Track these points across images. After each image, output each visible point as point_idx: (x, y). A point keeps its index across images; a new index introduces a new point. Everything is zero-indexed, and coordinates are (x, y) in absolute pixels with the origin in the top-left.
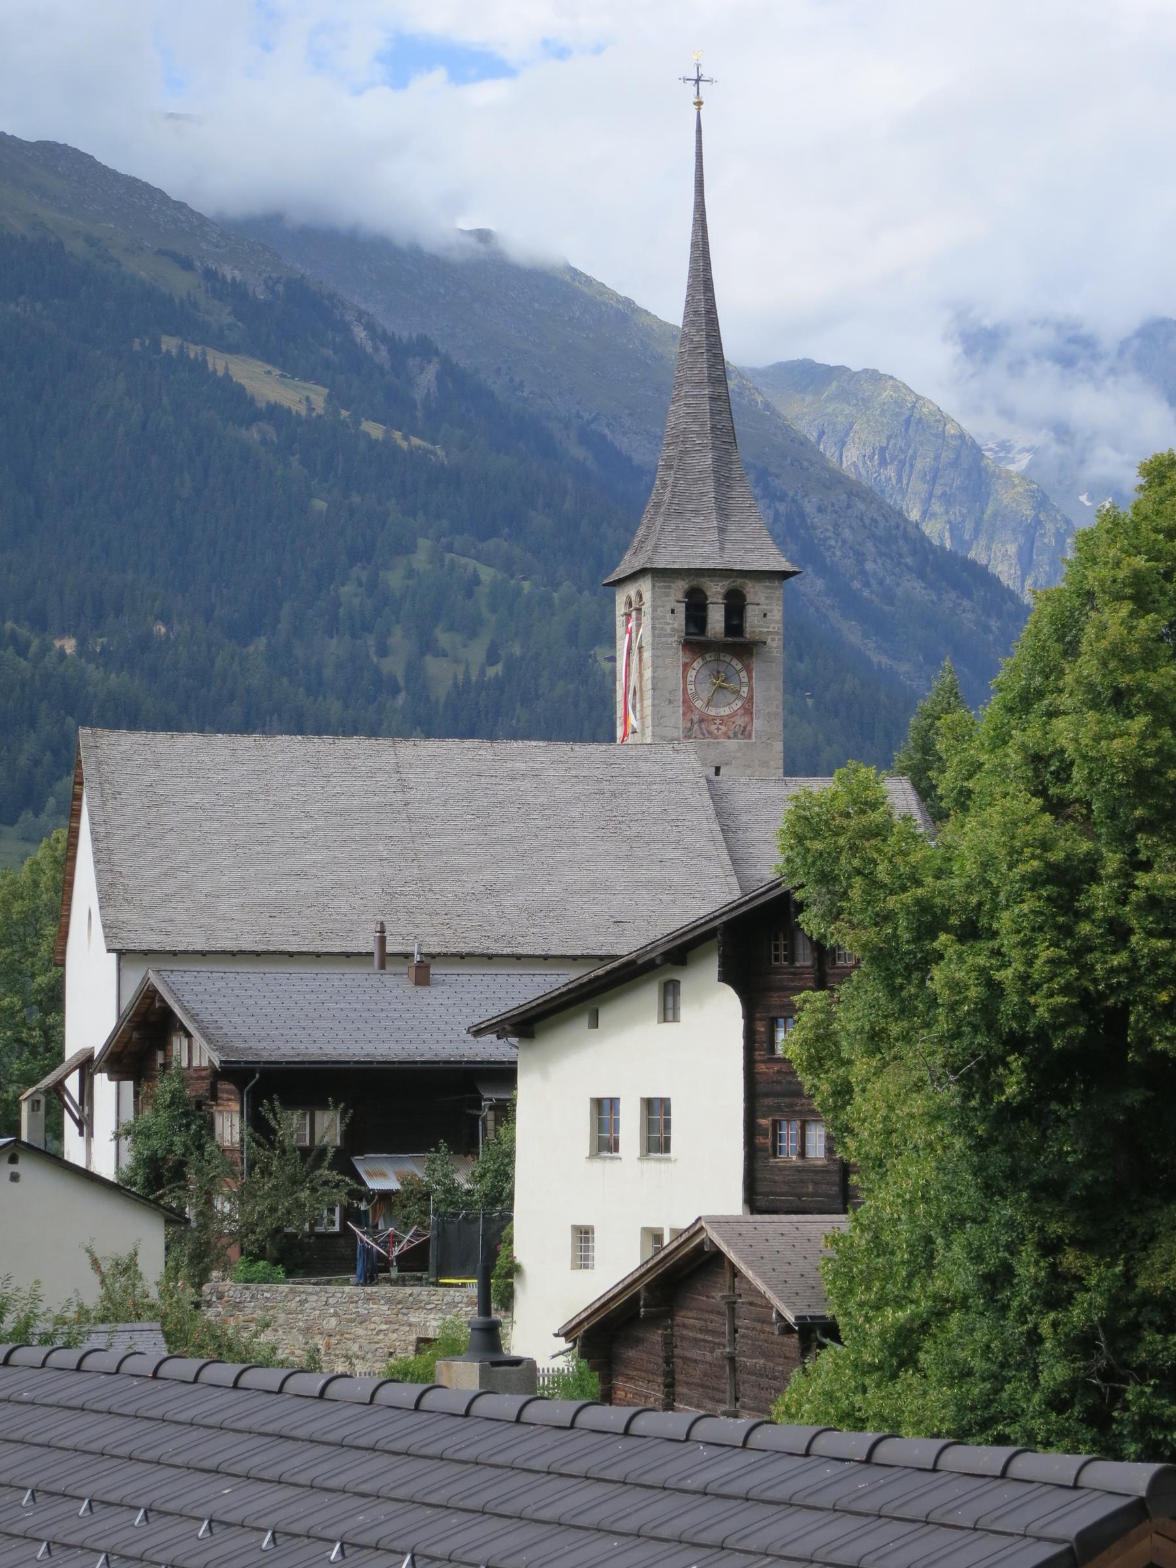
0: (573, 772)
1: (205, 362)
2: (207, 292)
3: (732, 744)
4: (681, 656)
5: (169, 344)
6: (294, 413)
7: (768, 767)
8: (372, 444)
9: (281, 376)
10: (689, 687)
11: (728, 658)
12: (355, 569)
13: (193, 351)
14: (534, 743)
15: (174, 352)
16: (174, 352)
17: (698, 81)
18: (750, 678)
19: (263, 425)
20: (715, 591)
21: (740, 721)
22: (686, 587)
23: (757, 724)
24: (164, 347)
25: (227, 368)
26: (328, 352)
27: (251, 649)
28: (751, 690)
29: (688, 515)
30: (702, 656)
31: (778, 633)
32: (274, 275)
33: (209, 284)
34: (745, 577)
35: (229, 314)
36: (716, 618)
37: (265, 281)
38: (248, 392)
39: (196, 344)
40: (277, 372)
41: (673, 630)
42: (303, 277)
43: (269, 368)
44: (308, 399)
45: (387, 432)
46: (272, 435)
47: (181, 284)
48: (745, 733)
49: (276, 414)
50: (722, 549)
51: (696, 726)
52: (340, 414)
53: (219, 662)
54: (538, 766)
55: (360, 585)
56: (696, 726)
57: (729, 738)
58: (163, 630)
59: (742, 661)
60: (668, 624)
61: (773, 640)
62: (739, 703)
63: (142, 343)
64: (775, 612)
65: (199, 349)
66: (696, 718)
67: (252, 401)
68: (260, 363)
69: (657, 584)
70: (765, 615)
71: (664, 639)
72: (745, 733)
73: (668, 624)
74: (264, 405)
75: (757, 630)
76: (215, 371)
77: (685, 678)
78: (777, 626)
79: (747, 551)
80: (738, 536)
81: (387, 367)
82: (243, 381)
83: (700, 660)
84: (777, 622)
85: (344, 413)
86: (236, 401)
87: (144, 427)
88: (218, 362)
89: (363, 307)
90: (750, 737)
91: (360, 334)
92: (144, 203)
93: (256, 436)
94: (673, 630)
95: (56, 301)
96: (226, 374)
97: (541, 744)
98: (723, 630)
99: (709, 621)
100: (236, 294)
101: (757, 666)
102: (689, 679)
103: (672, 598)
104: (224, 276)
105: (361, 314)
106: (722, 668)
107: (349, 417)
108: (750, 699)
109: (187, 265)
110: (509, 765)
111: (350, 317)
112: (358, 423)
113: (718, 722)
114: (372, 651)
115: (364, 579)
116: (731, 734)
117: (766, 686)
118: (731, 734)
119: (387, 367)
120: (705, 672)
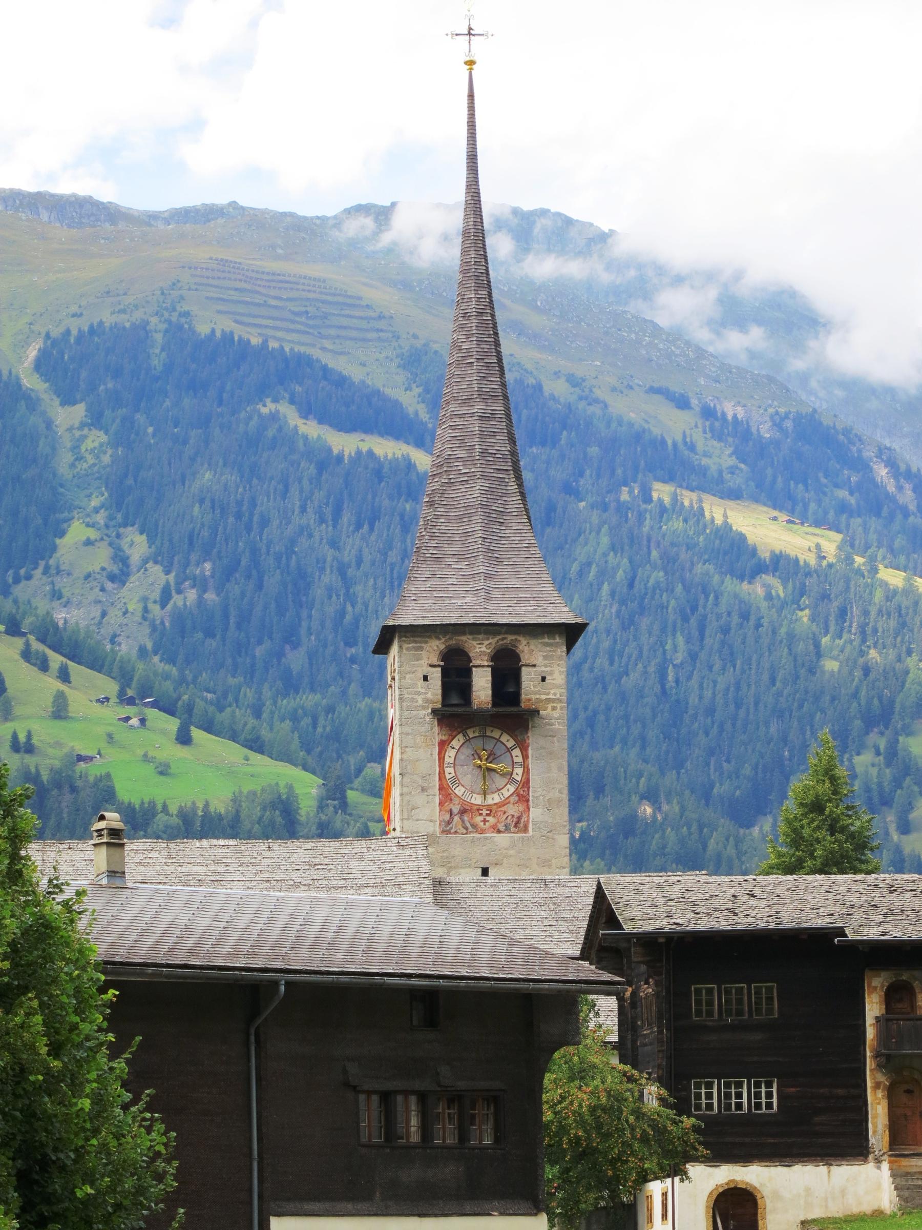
0: (265, 876)
1: (702, 509)
2: (705, 432)
3: (503, 839)
4: (436, 734)
5: (662, 492)
6: (802, 563)
7: (550, 866)
8: (891, 594)
9: (789, 522)
10: (447, 770)
11: (496, 734)
12: (871, 735)
13: (688, 498)
14: (221, 842)
15: (667, 500)
16: (667, 500)
17: (470, 34)
18: (525, 757)
19: (768, 579)
20: (480, 651)
21: (513, 810)
22: (442, 647)
23: (535, 813)
24: (655, 495)
25: (725, 516)
26: (843, 494)
27: (756, 831)
28: (526, 771)
29: (450, 561)
30: (463, 731)
31: (560, 701)
32: (782, 410)
33: (708, 423)
34: (518, 634)
35: (730, 456)
36: (482, 686)
37: (772, 417)
38: (750, 542)
39: (692, 490)
40: (783, 517)
41: (427, 701)
42: (815, 411)
43: (775, 513)
44: (818, 546)
45: (907, 580)
46: (779, 589)
47: (675, 425)
48: (520, 825)
49: (780, 564)
50: (488, 599)
51: (456, 818)
52: (853, 561)
53: (712, 844)
54: (221, 869)
55: (878, 753)
56: (456, 818)
57: (499, 832)
58: (649, 810)
59: (514, 737)
60: (419, 693)
61: (554, 708)
62: (512, 788)
63: (631, 492)
64: (556, 674)
65: (694, 496)
66: (456, 810)
67: (754, 552)
68: (765, 509)
69: (405, 646)
70: (544, 679)
71: (414, 713)
72: (520, 825)
73: (419, 693)
74: (767, 555)
75: (533, 697)
76: (713, 520)
77: (441, 759)
78: (558, 691)
79: (520, 600)
80: (511, 583)
81: (912, 507)
82: (743, 530)
83: (460, 736)
84: (558, 687)
85: (859, 560)
86: (738, 556)
87: (631, 585)
88: (717, 511)
89: (887, 442)
90: (525, 829)
91: (882, 472)
92: (633, 336)
93: (760, 591)
94: (427, 701)
95: (534, 450)
96: (726, 523)
97: (232, 842)
98: (490, 699)
99: (474, 689)
100: (739, 434)
101: (534, 740)
102: (447, 760)
103: (424, 662)
104: (724, 414)
105: (881, 451)
106: (490, 745)
107: (864, 564)
108: (526, 783)
109: (682, 403)
110: (183, 869)
111: (869, 453)
112: (875, 570)
113: (484, 812)
114: (892, 829)
115: (882, 748)
116: (501, 827)
117: (546, 766)
118: (501, 827)
119: (912, 507)
120: (467, 751)
